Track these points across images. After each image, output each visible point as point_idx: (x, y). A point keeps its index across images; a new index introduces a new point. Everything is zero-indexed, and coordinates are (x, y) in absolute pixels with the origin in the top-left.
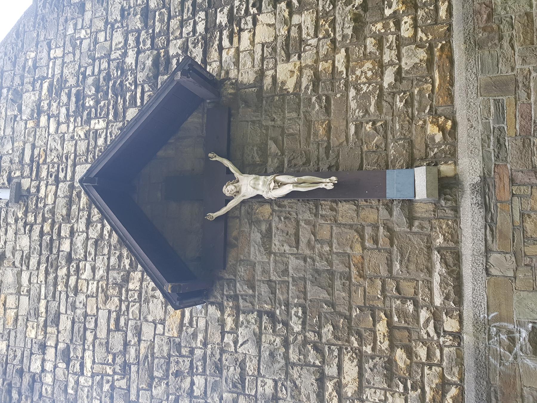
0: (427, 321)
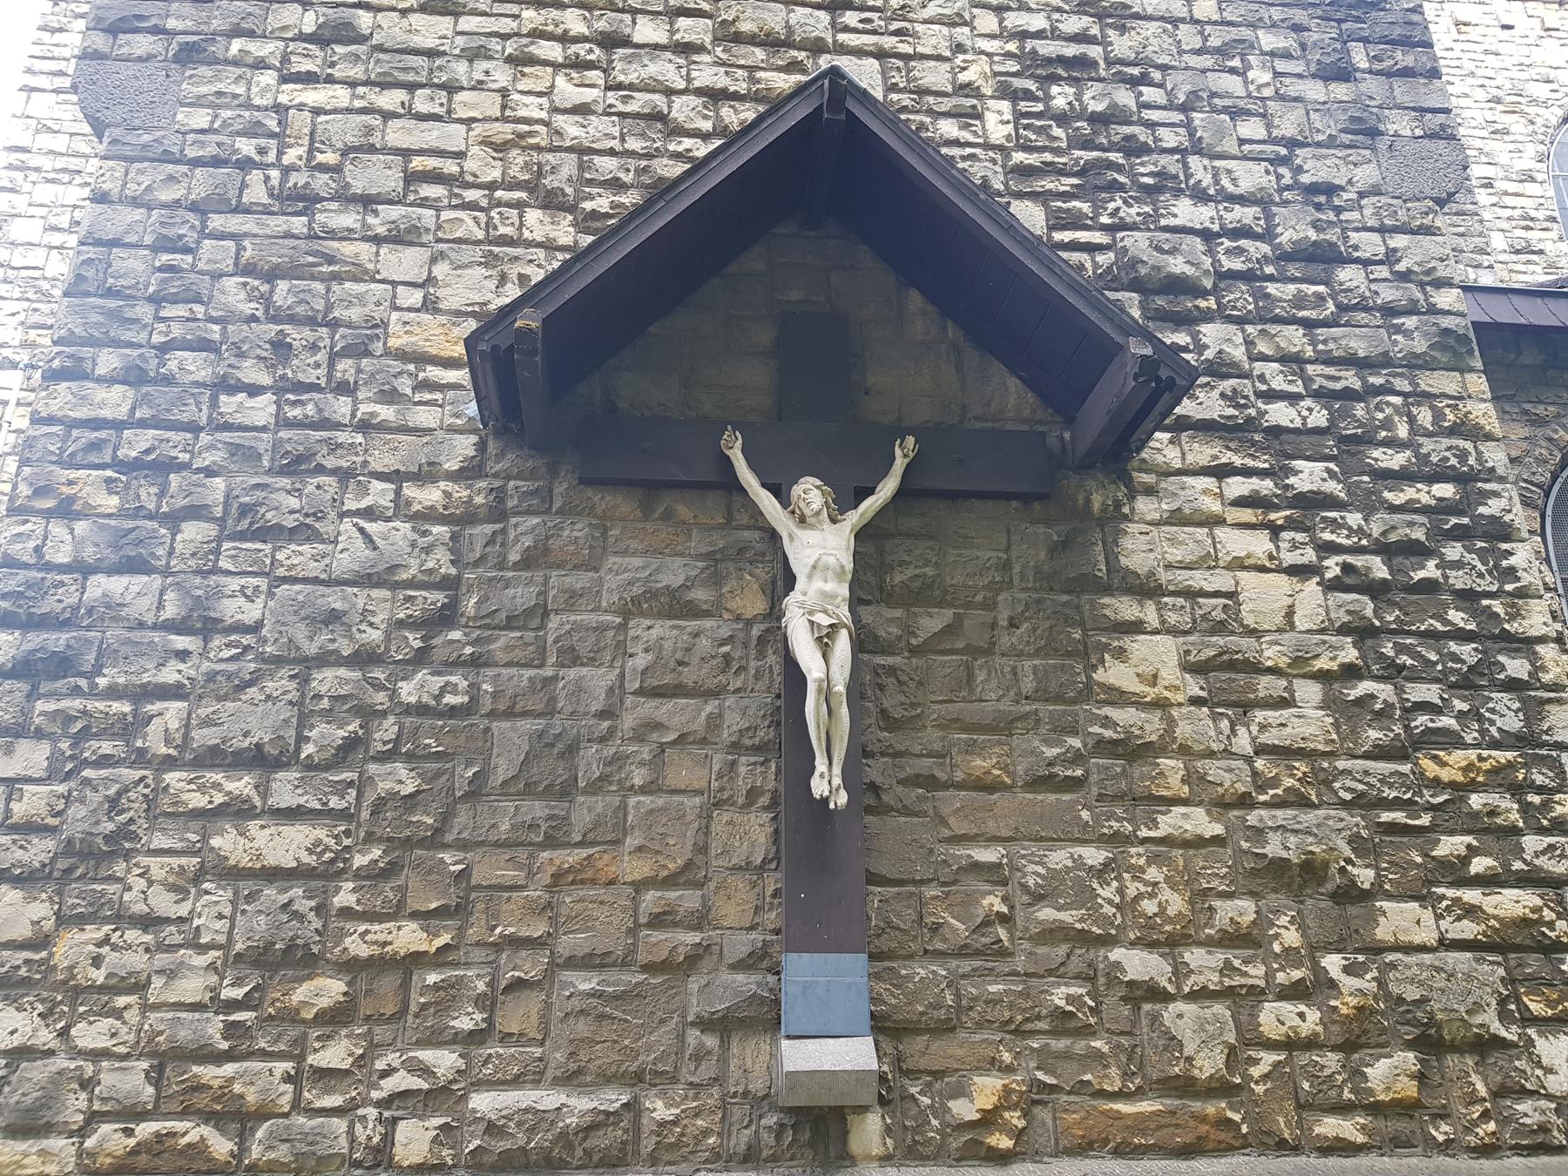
0: (425, 1071)
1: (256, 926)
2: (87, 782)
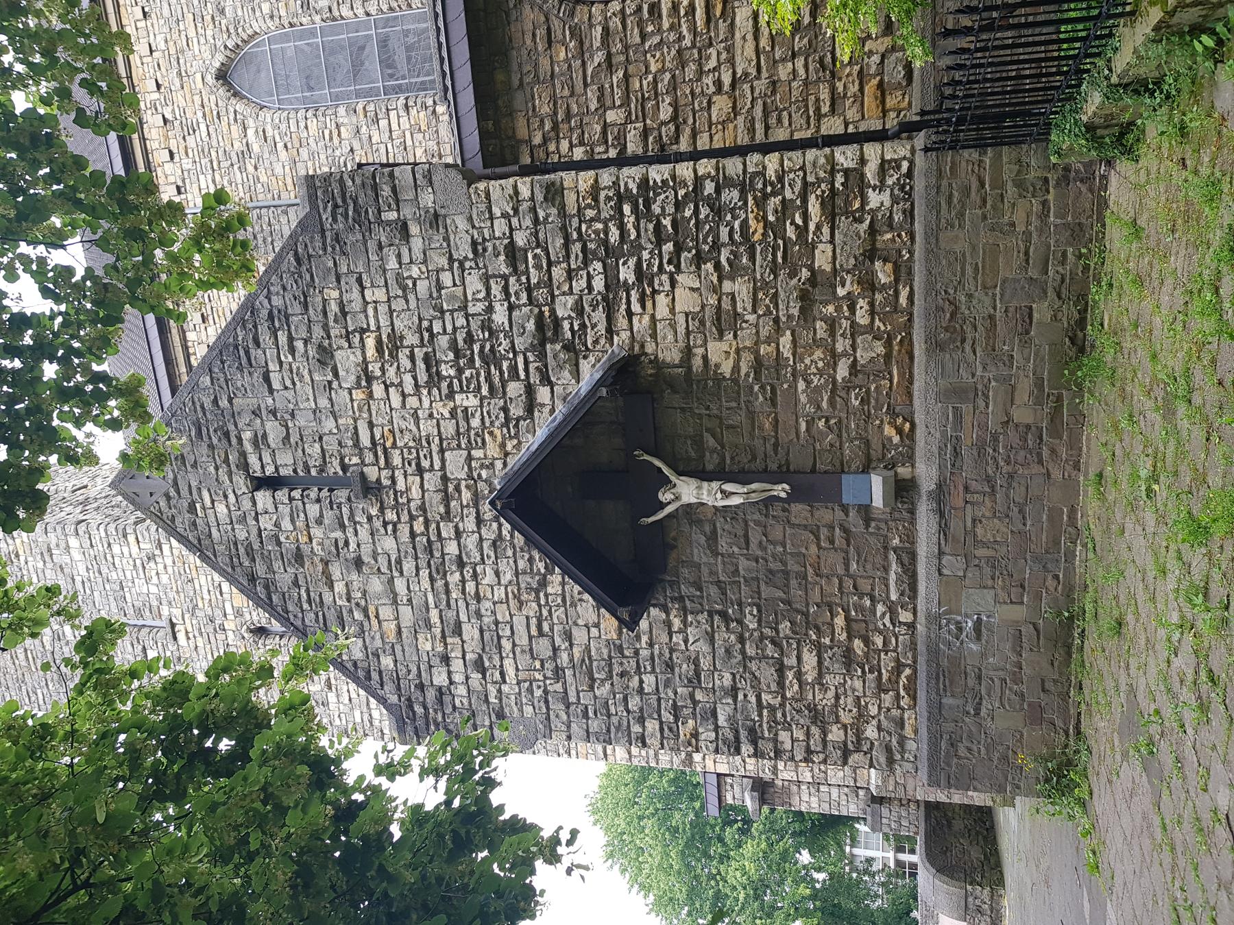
0: (884, 614)
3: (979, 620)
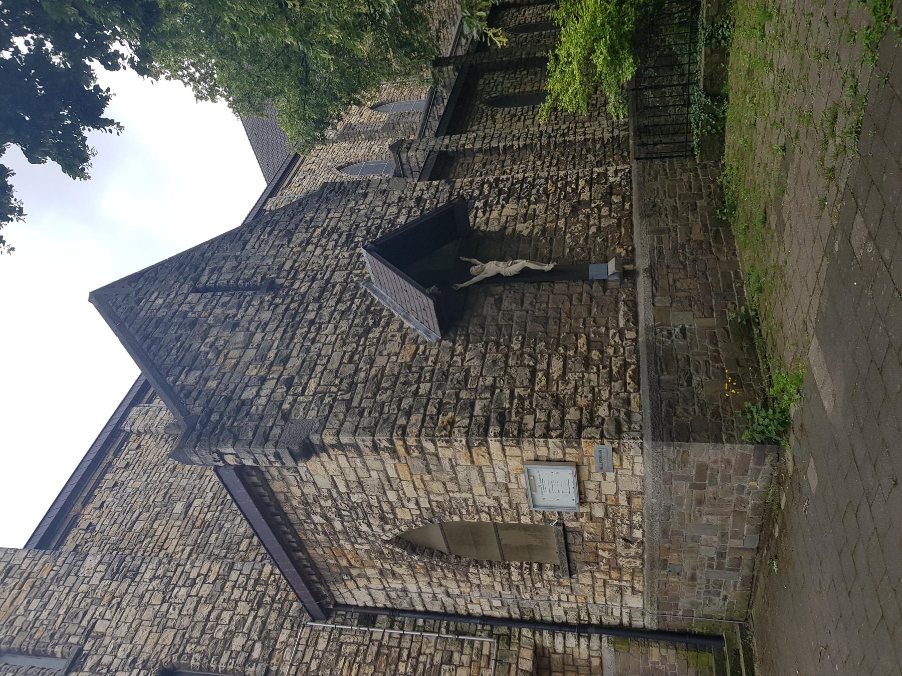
0: (615, 334)
1: (579, 367)
2: (536, 406)
3: (683, 327)
